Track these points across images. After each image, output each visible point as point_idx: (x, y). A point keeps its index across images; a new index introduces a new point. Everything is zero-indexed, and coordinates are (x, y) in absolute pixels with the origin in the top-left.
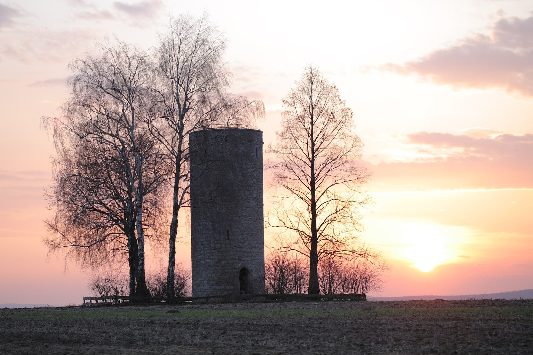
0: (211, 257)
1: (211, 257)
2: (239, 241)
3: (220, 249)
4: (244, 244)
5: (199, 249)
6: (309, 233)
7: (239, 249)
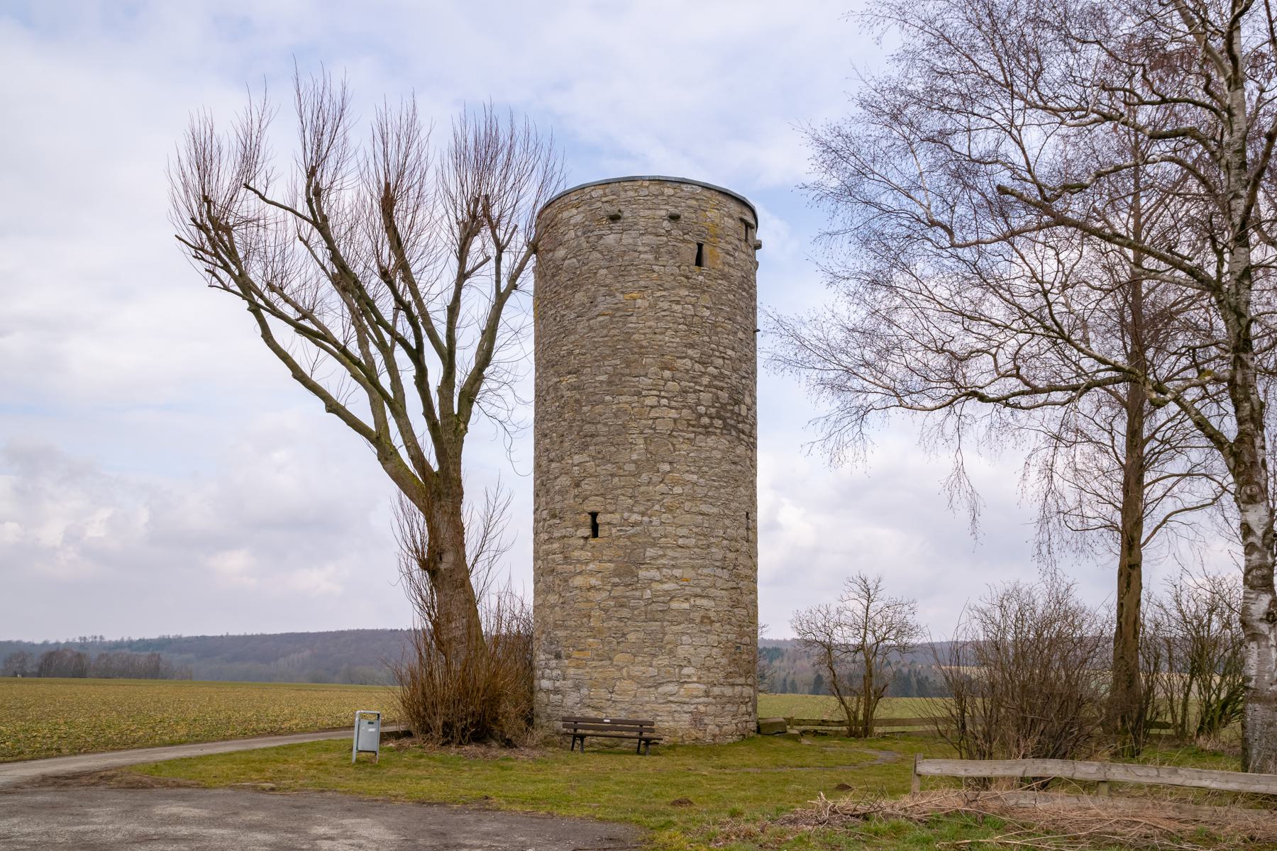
0: (713, 592)
1: (713, 592)
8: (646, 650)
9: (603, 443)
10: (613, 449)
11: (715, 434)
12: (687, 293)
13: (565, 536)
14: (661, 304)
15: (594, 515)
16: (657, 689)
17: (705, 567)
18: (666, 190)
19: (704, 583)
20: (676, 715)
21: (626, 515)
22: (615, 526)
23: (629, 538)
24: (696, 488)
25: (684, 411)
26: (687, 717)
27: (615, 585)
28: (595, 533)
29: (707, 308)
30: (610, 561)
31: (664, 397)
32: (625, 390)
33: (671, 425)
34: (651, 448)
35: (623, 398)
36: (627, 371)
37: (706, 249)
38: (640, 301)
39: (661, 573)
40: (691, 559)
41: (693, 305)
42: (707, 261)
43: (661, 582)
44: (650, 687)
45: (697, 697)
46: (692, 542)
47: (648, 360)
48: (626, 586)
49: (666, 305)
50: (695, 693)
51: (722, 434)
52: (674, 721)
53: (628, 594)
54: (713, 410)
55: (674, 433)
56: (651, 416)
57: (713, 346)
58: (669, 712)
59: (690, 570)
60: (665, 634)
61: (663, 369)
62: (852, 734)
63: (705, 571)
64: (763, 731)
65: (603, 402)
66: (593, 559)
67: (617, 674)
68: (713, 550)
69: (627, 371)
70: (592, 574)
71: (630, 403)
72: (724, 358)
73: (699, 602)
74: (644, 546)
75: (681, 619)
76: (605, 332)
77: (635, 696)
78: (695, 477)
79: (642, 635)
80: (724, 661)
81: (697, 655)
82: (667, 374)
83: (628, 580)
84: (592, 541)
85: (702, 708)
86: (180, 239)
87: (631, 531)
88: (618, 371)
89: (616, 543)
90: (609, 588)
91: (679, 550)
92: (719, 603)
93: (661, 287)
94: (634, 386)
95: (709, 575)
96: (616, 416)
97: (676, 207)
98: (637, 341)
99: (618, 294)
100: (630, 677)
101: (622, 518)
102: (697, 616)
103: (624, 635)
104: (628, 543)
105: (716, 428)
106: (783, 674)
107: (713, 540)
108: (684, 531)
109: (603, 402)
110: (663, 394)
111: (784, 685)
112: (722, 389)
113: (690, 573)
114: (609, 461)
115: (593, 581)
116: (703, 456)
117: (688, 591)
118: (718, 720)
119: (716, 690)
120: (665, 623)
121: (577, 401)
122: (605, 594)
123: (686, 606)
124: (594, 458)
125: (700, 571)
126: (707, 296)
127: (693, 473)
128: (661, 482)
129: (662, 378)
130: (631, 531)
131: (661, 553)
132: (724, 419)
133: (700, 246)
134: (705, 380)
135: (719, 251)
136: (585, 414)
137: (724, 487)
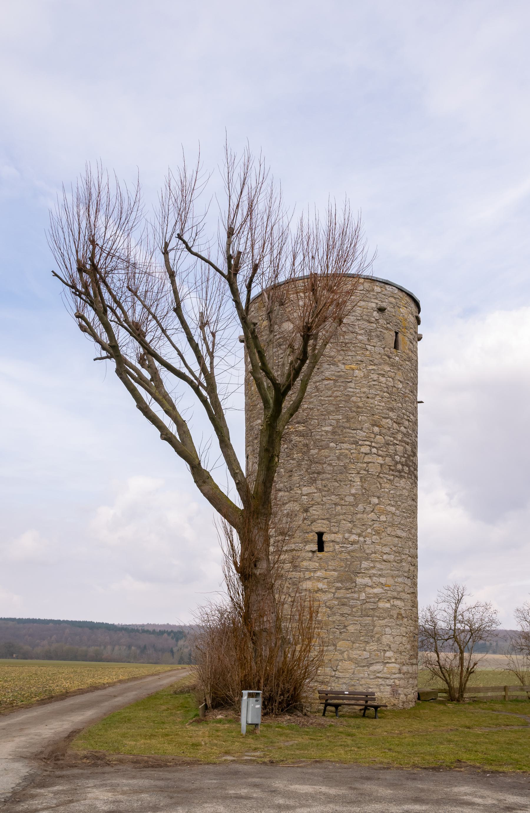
8: (362, 638)
9: (328, 479)
10: (336, 484)
12: (389, 369)
13: (294, 550)
14: (372, 376)
15: (320, 535)
16: (369, 668)
17: (399, 576)
18: (375, 288)
20: (382, 687)
21: (347, 535)
22: (338, 543)
23: (349, 553)
24: (394, 517)
25: (387, 458)
26: (388, 689)
27: (338, 589)
28: (321, 548)
29: (401, 382)
30: (334, 570)
31: (374, 447)
32: (346, 439)
33: (379, 469)
34: (365, 485)
35: (345, 446)
36: (347, 425)
38: (357, 371)
39: (372, 580)
40: (391, 570)
41: (393, 379)
42: (401, 346)
43: (372, 587)
44: (364, 666)
46: (391, 557)
47: (363, 418)
48: (347, 589)
49: (375, 377)
50: (393, 671)
51: (408, 477)
52: (381, 692)
53: (348, 595)
54: (404, 459)
55: (381, 475)
56: (365, 460)
57: (404, 411)
58: (377, 685)
59: (390, 578)
60: (374, 626)
61: (373, 425)
62: (452, 699)
64: (422, 698)
65: (327, 447)
66: (320, 568)
67: (340, 657)
68: (404, 564)
69: (347, 425)
70: (319, 579)
71: (350, 450)
74: (361, 559)
75: (385, 615)
76: (330, 393)
77: (353, 673)
78: (394, 509)
79: (358, 627)
80: (409, 647)
81: (394, 642)
82: (376, 429)
83: (348, 585)
84: (320, 554)
85: (397, 682)
86: (56, 275)
87: (351, 548)
88: (341, 424)
89: (339, 556)
90: (333, 591)
91: (384, 563)
93: (372, 362)
94: (352, 437)
96: (338, 458)
97: (382, 302)
98: (355, 402)
99: (340, 365)
100: (350, 659)
101: (344, 537)
102: (394, 613)
103: (345, 627)
104: (349, 557)
105: (406, 473)
106: (186, 650)
107: (403, 557)
108: (387, 550)
109: (327, 447)
110: (373, 444)
111: (190, 659)
113: (390, 581)
114: (333, 493)
115: (320, 585)
116: (398, 494)
117: (390, 594)
118: (406, 690)
119: (405, 669)
120: (375, 618)
121: (306, 445)
122: (330, 596)
123: (388, 605)
124: (320, 490)
126: (400, 373)
127: (393, 506)
128: (372, 511)
129: (373, 432)
130: (351, 548)
131: (372, 565)
134: (400, 436)
135: (407, 339)
136: (313, 455)
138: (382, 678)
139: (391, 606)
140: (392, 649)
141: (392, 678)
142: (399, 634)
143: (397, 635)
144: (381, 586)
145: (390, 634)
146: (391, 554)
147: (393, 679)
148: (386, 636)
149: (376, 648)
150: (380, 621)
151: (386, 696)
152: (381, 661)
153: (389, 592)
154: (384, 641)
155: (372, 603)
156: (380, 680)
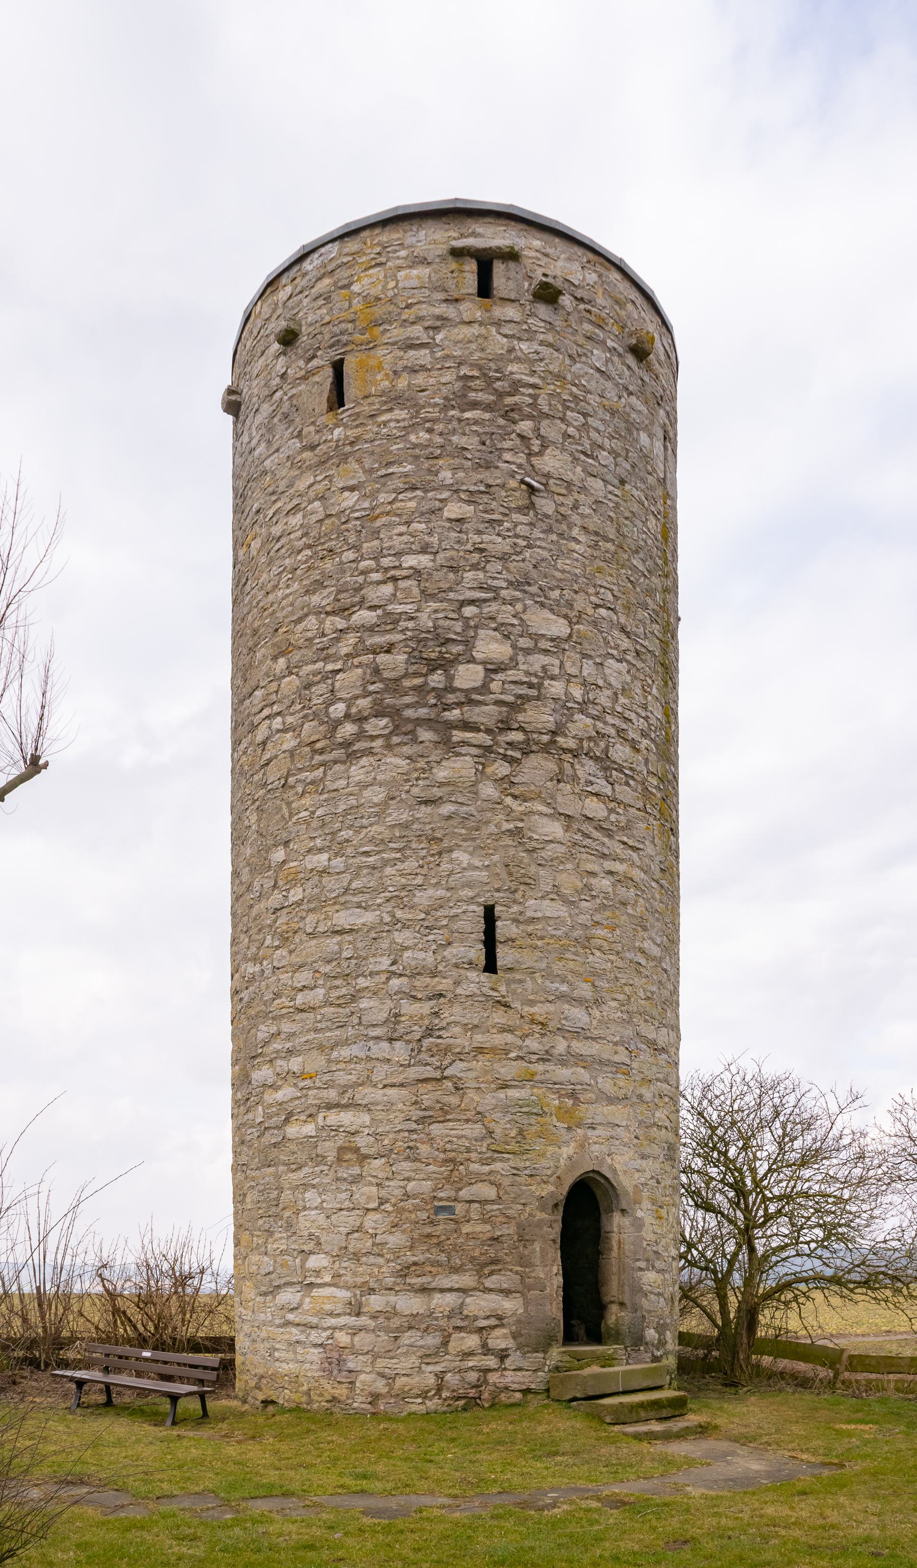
0: (366, 1094)
1: (366, 1094)
2: (564, 988)
3: (429, 1032)
4: (596, 1013)
5: (276, 1045)
6: (431, 1287)
7: (561, 1046)
11: (369, 752)
17: (346, 1042)
19: (343, 1078)
20: (299, 1349)
26: (315, 1354)
37: (349, 368)
40: (316, 1030)
45: (331, 1314)
50: (328, 1307)
51: (389, 747)
59: (315, 1053)
63: (345, 1052)
68: (364, 1004)
72: (394, 579)
73: (333, 1118)
75: (301, 1157)
78: (324, 857)
80: (396, 1239)
85: (343, 1338)
91: (298, 1017)
92: (381, 1116)
95: (357, 1060)
102: (329, 1148)
105: (373, 738)
107: (362, 982)
108: (304, 977)
112: (389, 649)
113: (316, 1062)
116: (342, 807)
118: (381, 1363)
119: (376, 1302)
123: (309, 1129)
125: (335, 1054)
132: (394, 713)
133: (338, 367)
137: (394, 862)
138: (298, 1325)
139: (317, 1129)
140: (326, 1248)
141: (325, 1326)
142: (347, 1204)
143: (341, 1209)
144: (292, 1080)
145: (316, 1208)
146: (315, 987)
147: (329, 1328)
148: (306, 1213)
149: (284, 1247)
150: (291, 1175)
151: (309, 1374)
152: (295, 1280)
153: (310, 1092)
154: (302, 1228)
155: (274, 1128)
156: (294, 1330)
